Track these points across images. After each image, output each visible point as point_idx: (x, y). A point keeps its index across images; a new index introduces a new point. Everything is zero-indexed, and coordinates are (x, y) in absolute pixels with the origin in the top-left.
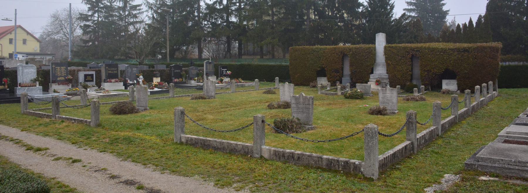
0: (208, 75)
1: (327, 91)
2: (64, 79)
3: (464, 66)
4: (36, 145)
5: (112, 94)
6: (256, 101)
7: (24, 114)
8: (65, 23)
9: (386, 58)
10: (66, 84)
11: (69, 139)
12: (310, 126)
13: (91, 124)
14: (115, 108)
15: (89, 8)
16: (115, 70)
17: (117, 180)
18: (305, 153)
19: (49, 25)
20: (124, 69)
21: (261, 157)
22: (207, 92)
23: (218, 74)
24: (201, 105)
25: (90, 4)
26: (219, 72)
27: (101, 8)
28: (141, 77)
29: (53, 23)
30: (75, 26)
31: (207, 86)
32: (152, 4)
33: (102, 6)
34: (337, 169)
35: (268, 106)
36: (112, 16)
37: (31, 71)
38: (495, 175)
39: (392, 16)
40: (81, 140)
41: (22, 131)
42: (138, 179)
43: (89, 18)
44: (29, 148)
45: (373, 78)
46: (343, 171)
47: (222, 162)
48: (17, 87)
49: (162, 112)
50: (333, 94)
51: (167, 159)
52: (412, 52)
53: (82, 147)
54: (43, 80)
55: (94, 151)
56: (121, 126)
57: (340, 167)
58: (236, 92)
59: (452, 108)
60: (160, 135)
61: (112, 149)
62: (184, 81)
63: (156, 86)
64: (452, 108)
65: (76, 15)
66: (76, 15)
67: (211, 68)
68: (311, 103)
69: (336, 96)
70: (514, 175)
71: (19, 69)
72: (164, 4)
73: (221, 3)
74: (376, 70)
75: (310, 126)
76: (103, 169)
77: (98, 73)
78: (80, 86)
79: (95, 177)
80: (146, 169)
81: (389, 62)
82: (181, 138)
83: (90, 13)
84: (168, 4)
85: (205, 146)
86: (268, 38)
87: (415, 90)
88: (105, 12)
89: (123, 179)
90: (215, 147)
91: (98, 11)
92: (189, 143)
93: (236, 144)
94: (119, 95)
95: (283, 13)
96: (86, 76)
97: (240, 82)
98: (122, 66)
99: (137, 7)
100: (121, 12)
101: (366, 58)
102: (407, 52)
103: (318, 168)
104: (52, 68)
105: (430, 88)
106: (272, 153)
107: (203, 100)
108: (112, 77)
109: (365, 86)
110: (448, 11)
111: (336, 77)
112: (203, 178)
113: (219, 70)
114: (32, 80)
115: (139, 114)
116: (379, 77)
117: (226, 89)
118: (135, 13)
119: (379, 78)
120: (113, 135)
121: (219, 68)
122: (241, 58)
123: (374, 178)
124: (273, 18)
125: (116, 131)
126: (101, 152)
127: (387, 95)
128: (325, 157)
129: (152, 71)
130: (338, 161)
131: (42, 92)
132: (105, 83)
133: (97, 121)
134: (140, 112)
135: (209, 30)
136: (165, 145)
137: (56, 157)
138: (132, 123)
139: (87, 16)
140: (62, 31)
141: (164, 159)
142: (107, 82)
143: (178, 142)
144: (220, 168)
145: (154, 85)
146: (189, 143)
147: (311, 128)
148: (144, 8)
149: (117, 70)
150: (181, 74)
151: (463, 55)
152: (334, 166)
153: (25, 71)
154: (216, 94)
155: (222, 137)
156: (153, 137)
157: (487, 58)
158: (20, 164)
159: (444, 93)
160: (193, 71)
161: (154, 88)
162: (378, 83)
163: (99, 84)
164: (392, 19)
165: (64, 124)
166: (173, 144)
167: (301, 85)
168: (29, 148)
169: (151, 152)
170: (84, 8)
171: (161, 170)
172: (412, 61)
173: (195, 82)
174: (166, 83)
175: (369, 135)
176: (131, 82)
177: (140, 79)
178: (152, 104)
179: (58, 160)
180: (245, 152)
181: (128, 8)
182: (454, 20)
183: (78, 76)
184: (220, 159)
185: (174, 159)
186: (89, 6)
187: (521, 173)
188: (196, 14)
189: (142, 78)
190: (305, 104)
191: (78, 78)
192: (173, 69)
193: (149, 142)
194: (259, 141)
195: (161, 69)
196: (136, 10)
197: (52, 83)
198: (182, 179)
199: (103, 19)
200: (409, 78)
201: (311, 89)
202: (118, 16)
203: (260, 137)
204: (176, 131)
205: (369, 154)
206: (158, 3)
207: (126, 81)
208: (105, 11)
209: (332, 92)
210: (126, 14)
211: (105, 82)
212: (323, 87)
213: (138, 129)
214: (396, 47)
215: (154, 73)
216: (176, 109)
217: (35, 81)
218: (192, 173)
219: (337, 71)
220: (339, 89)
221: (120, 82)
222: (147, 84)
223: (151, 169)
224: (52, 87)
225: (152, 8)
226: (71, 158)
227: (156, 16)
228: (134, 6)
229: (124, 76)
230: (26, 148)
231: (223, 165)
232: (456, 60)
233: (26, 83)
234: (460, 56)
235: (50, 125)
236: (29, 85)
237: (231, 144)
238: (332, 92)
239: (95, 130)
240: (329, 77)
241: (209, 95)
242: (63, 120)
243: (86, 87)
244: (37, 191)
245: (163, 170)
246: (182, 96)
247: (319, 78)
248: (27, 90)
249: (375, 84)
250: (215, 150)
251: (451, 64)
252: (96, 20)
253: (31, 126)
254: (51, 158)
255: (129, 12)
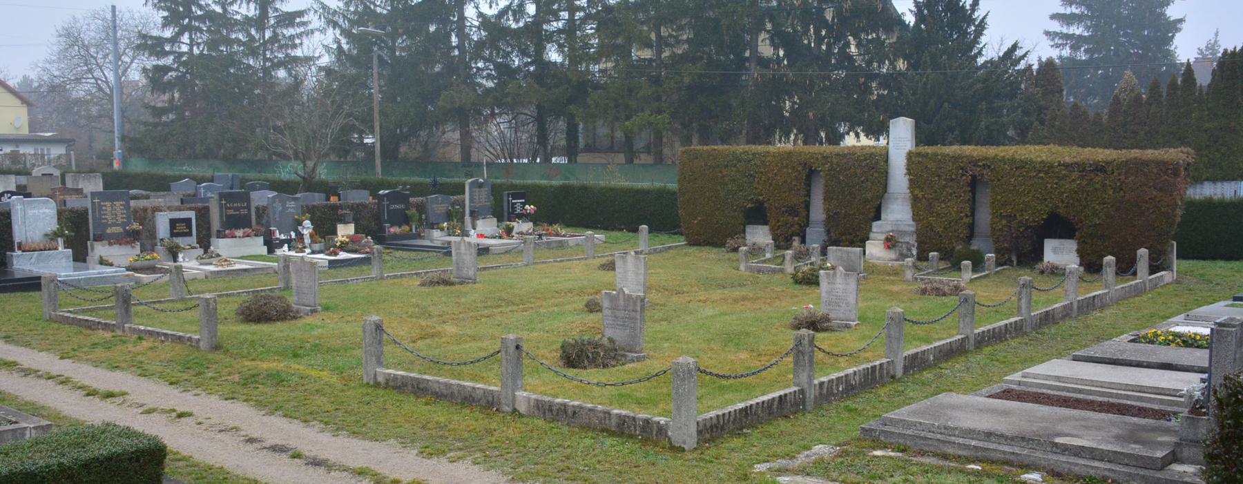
0: (474, 215)
1: (764, 262)
2: (121, 230)
3: (1093, 208)
4: (103, 387)
5: (238, 267)
6: (570, 291)
7: (50, 320)
8: (97, 53)
9: (910, 180)
10: (127, 243)
11: (162, 376)
12: (636, 355)
13: (201, 344)
14: (248, 308)
15: (165, 18)
16: (244, 208)
17: (258, 445)
18: (584, 405)
19: (54, 58)
20: (265, 204)
21: (515, 410)
22: (458, 269)
23: (502, 213)
24: (440, 299)
25: (168, 9)
26: (505, 208)
27: (199, 18)
28: (307, 223)
29: (63, 55)
30: (127, 63)
31: (457, 254)
32: (335, 11)
33: (199, 13)
34: (633, 432)
35: (587, 305)
36: (229, 42)
37: (44, 213)
38: (902, 447)
39: (980, 53)
40: (186, 376)
41: (62, 358)
42: (292, 443)
43: (167, 48)
44: (91, 393)
45: (879, 230)
46: (642, 435)
47: (442, 419)
48: (14, 251)
49: (349, 319)
50: (774, 271)
51: (346, 412)
52: (974, 168)
53: (189, 391)
54: (73, 234)
55: (214, 398)
56: (261, 349)
57: (637, 428)
58: (535, 263)
59: (961, 320)
60: (338, 368)
61: (247, 395)
62: (414, 231)
63: (343, 246)
64: (961, 320)
65: (126, 30)
66: (126, 30)
67: (484, 197)
68: (639, 309)
69: (782, 275)
70: (932, 449)
71: (17, 210)
72: (367, 16)
73: (519, 11)
74: (889, 211)
75: (636, 355)
76: (232, 429)
77: (203, 214)
78: (159, 247)
79: (221, 440)
80: (307, 430)
81: (916, 192)
82: (375, 375)
83: (168, 33)
84: (379, 10)
85: (419, 389)
86: (643, 110)
87: (965, 265)
88: (209, 31)
89: (267, 444)
90: (436, 393)
91: (189, 28)
92: (391, 384)
93: (474, 388)
94: (254, 270)
95: (688, 41)
96: (173, 223)
97: (558, 235)
98: (261, 197)
99: (295, 19)
100: (253, 32)
101: (862, 182)
102: (962, 169)
103: (603, 430)
104: (93, 204)
105: (1014, 259)
106: (532, 404)
107: (448, 287)
108: (235, 223)
109: (848, 252)
110: (1181, 21)
111: (792, 226)
112: (403, 443)
113: (505, 204)
114: (46, 235)
115: (299, 323)
116: (895, 228)
117: (518, 252)
118: (289, 34)
119: (892, 231)
120: (246, 369)
121: (505, 198)
122: (576, 161)
123: (686, 447)
124: (659, 52)
125: (253, 360)
126: (226, 399)
127: (838, 286)
128: (616, 411)
129: (334, 208)
130: (634, 419)
131: (71, 263)
132: (221, 240)
133: (214, 339)
134: (301, 317)
135: (490, 84)
136: (345, 388)
137: (145, 408)
138: (284, 342)
139: (160, 41)
140: (91, 76)
141: (340, 414)
142: (225, 237)
143: (372, 383)
144: (436, 428)
145: (338, 244)
146: (391, 384)
147: (637, 357)
148: (315, 21)
149: (249, 208)
150: (406, 214)
151: (1091, 180)
152: (629, 427)
153: (31, 212)
154: (479, 270)
155: (455, 373)
156: (325, 373)
157: (1146, 189)
158: (84, 419)
159: (1042, 272)
160: (438, 204)
161: (338, 251)
162: (889, 243)
163: (204, 243)
164: (981, 61)
165: (145, 344)
166: (362, 386)
167: (706, 245)
168: (91, 393)
169: (319, 400)
170: (154, 20)
171: (333, 431)
172: (973, 192)
173: (443, 233)
174: (369, 237)
175: (679, 376)
176: (283, 237)
177: (304, 227)
178: (328, 298)
179: (150, 413)
180: (488, 402)
181: (272, 22)
182: (1216, 42)
183: (154, 222)
184: (440, 414)
185: (359, 412)
186: (166, 14)
187: (941, 445)
188: (454, 40)
189: (310, 225)
190: (629, 311)
191: (154, 228)
192: (386, 203)
193: (315, 381)
194: (510, 383)
195: (357, 202)
196: (293, 27)
197: (95, 240)
198: (368, 444)
199: (203, 50)
200: (964, 232)
201: (727, 256)
202: (244, 44)
203: (515, 376)
204: (366, 362)
205: (678, 408)
206: (352, 9)
207: (271, 233)
208: (209, 28)
209: (773, 266)
210: (267, 37)
211: (218, 237)
212: (756, 251)
213: (296, 356)
214: (936, 155)
215: (340, 212)
216: (366, 320)
217: (55, 235)
218: (386, 436)
219: (793, 211)
220: (788, 258)
221: (256, 235)
222: (320, 242)
223: (316, 429)
224: (96, 250)
225: (335, 25)
226: (174, 410)
227: (348, 43)
228: (287, 13)
229: (264, 222)
230: (85, 392)
231: (442, 424)
232: (1076, 192)
233: (32, 242)
234: (1085, 183)
235: (115, 345)
236: (42, 248)
237: (464, 387)
238: (773, 266)
239: (210, 356)
240: (775, 225)
241: (464, 275)
242: (142, 335)
243: (173, 253)
244: (150, 448)
245: (336, 431)
246: (402, 276)
247: (751, 226)
248: (38, 260)
249: (882, 246)
250: (437, 398)
251: (1062, 201)
252: (186, 53)
253: (76, 348)
254: (136, 410)
255: (274, 32)
